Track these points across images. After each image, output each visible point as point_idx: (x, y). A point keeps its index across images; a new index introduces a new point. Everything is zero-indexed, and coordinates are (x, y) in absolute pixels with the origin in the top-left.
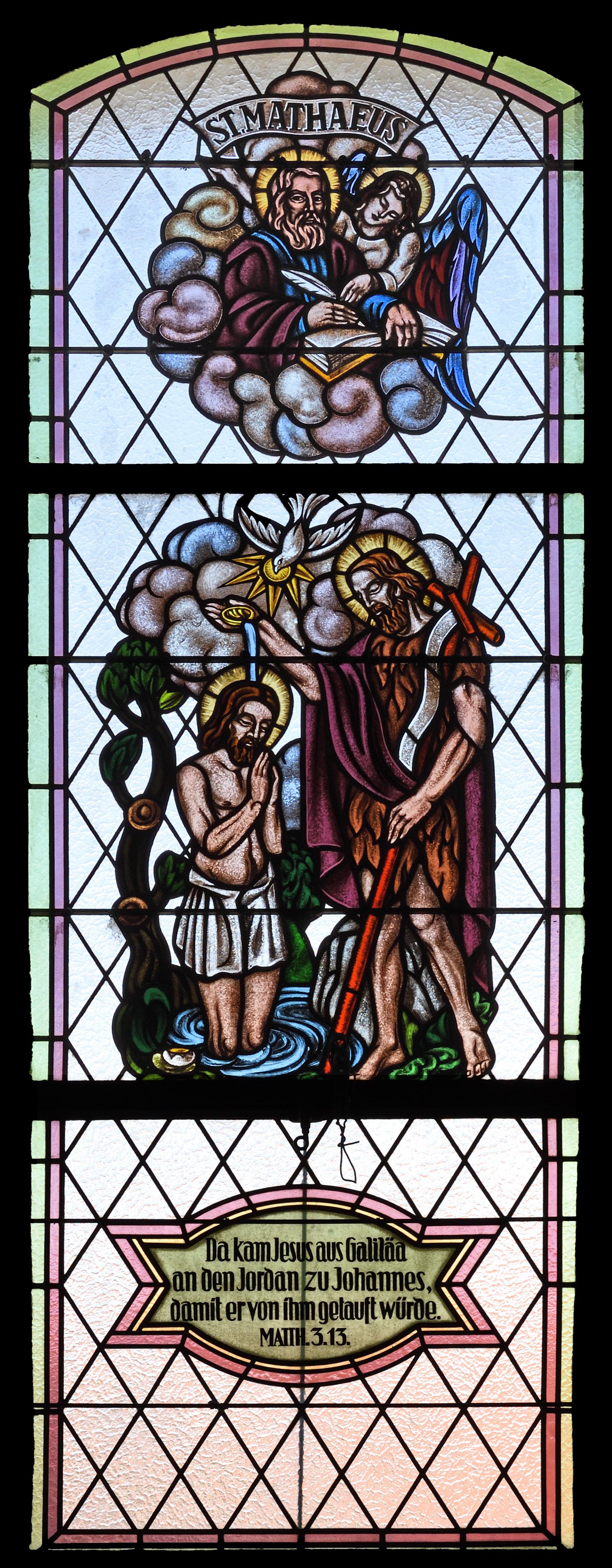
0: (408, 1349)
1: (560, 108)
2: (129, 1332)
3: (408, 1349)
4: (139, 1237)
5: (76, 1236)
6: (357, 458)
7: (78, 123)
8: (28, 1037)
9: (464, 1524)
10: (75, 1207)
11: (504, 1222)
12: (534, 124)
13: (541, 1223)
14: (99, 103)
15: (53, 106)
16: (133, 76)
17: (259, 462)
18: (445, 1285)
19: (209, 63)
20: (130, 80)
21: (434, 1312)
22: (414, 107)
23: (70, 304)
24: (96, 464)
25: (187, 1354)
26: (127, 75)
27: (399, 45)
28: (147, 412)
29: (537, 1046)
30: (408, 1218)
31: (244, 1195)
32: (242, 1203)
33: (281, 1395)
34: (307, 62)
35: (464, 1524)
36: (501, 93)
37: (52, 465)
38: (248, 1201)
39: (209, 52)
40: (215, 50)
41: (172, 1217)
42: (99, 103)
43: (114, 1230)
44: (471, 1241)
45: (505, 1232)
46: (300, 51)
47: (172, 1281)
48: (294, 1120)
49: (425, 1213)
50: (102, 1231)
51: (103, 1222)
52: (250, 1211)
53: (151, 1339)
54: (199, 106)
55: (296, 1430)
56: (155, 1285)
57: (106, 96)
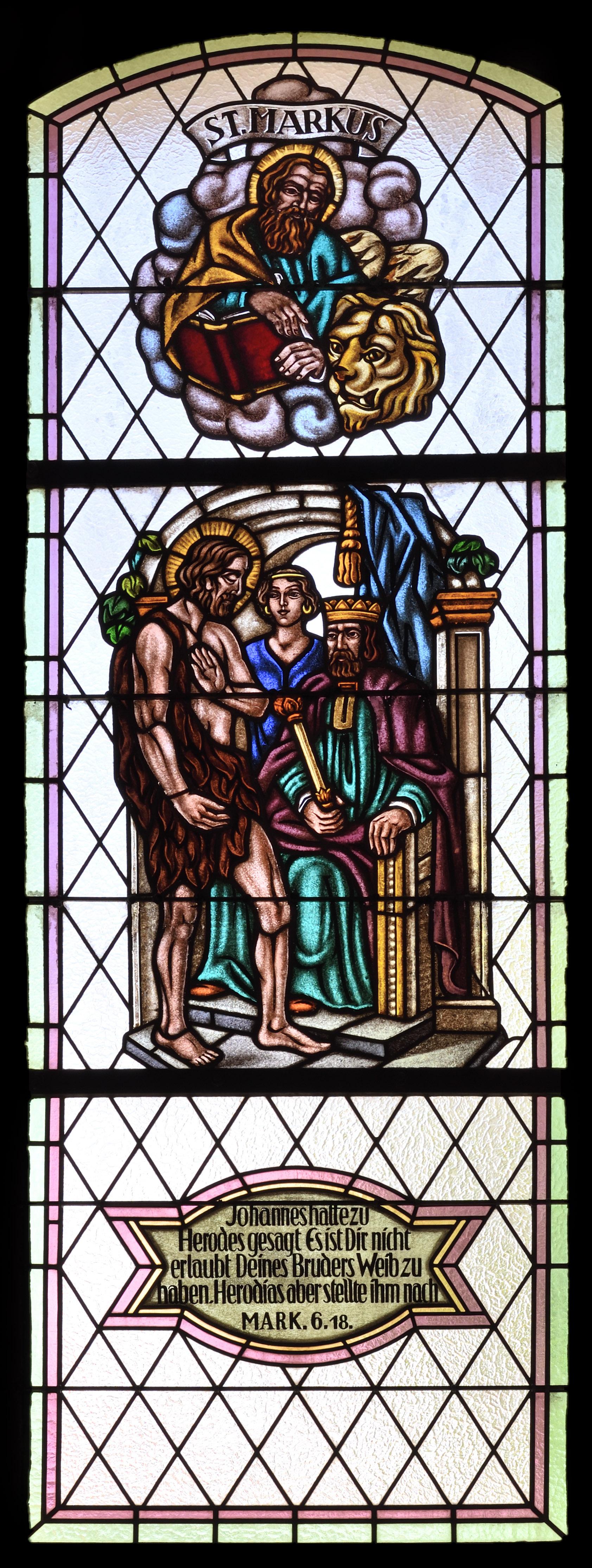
0: (399, 1331)
1: (542, 109)
3: (399, 1331)
4: (137, 1220)
5: (74, 1218)
7: (72, 134)
8: (23, 1023)
9: (376, 1501)
10: (74, 1190)
11: (494, 1204)
12: (516, 123)
14: (93, 115)
15: (48, 120)
16: (126, 90)
19: (199, 75)
20: (124, 94)
22: (402, 111)
23: (64, 1037)
26: (122, 89)
27: (385, 52)
31: (239, 1176)
32: (237, 1184)
33: (276, 1377)
34: (293, 68)
36: (484, 95)
39: (200, 64)
40: (206, 63)
42: (93, 115)
43: (113, 1212)
44: (463, 1222)
45: (496, 1213)
46: (286, 61)
47: (170, 1265)
51: (101, 1205)
52: (244, 1192)
54: (186, 117)
56: (153, 1267)
57: (100, 110)
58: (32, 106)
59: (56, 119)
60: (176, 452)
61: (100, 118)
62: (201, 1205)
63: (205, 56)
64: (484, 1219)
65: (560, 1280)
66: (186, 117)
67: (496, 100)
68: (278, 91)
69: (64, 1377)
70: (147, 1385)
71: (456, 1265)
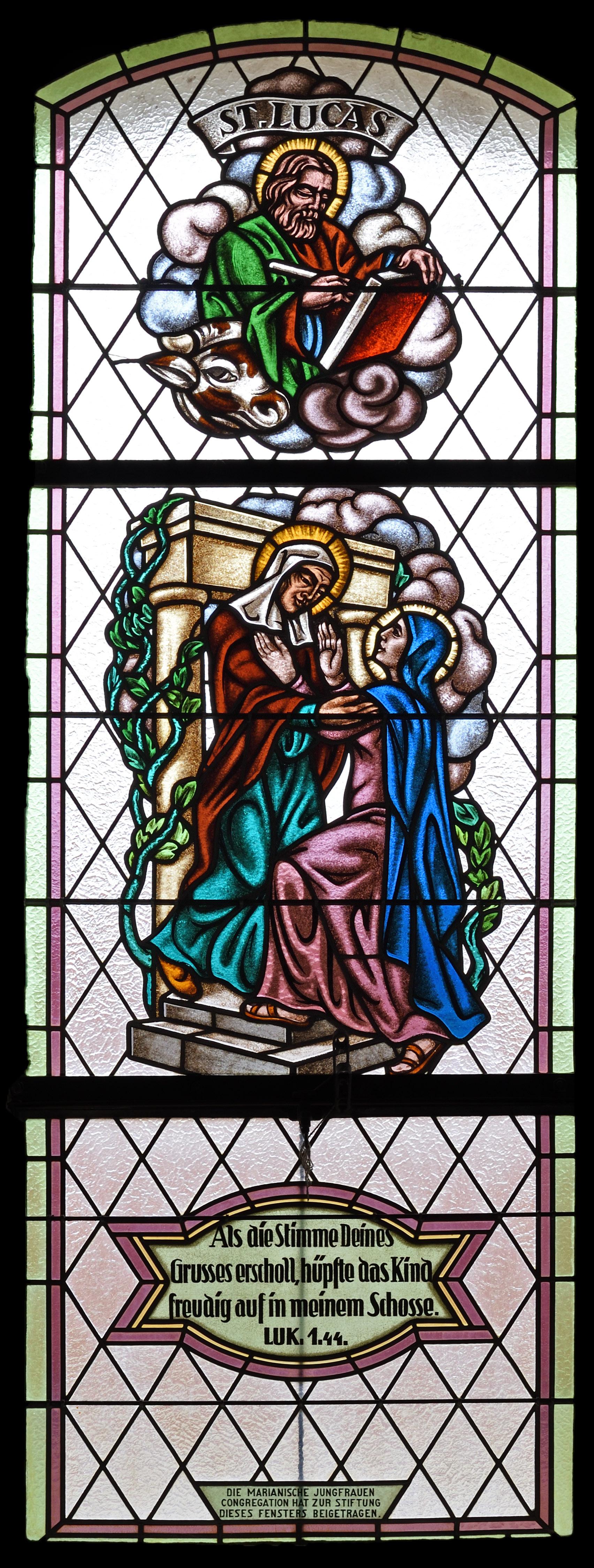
1: (555, 113)
2: (139, 1329)
6: (352, 453)
7: (79, 125)
11: (496, 1217)
12: (530, 127)
13: (558, 528)
14: (100, 106)
15: (55, 109)
17: (256, 457)
18: (441, 1280)
19: (207, 68)
20: (132, 84)
21: (431, 1309)
23: (67, 544)
24: (93, 460)
25: (188, 1350)
26: (130, 79)
28: (144, 408)
29: (532, 178)
30: (402, 1213)
33: (279, 1390)
34: (304, 62)
35: (459, 1514)
36: (496, 96)
37: (50, 461)
38: (247, 1198)
39: (209, 56)
40: (216, 55)
41: (171, 1213)
42: (100, 106)
46: (296, 55)
48: (293, 1119)
49: (420, 1210)
50: (103, 1229)
51: (105, 1220)
52: (248, 1208)
53: (149, 1337)
54: (194, 109)
55: (295, 1423)
57: (107, 100)
58: (40, 94)
59: (63, 108)
60: (183, 454)
61: (107, 109)
62: (207, 1220)
63: (214, 48)
64: (489, 1233)
65: (566, 1293)
66: (194, 109)
67: (508, 101)
68: (289, 82)
69: (67, 1391)
70: (153, 1399)
71: (460, 1280)
